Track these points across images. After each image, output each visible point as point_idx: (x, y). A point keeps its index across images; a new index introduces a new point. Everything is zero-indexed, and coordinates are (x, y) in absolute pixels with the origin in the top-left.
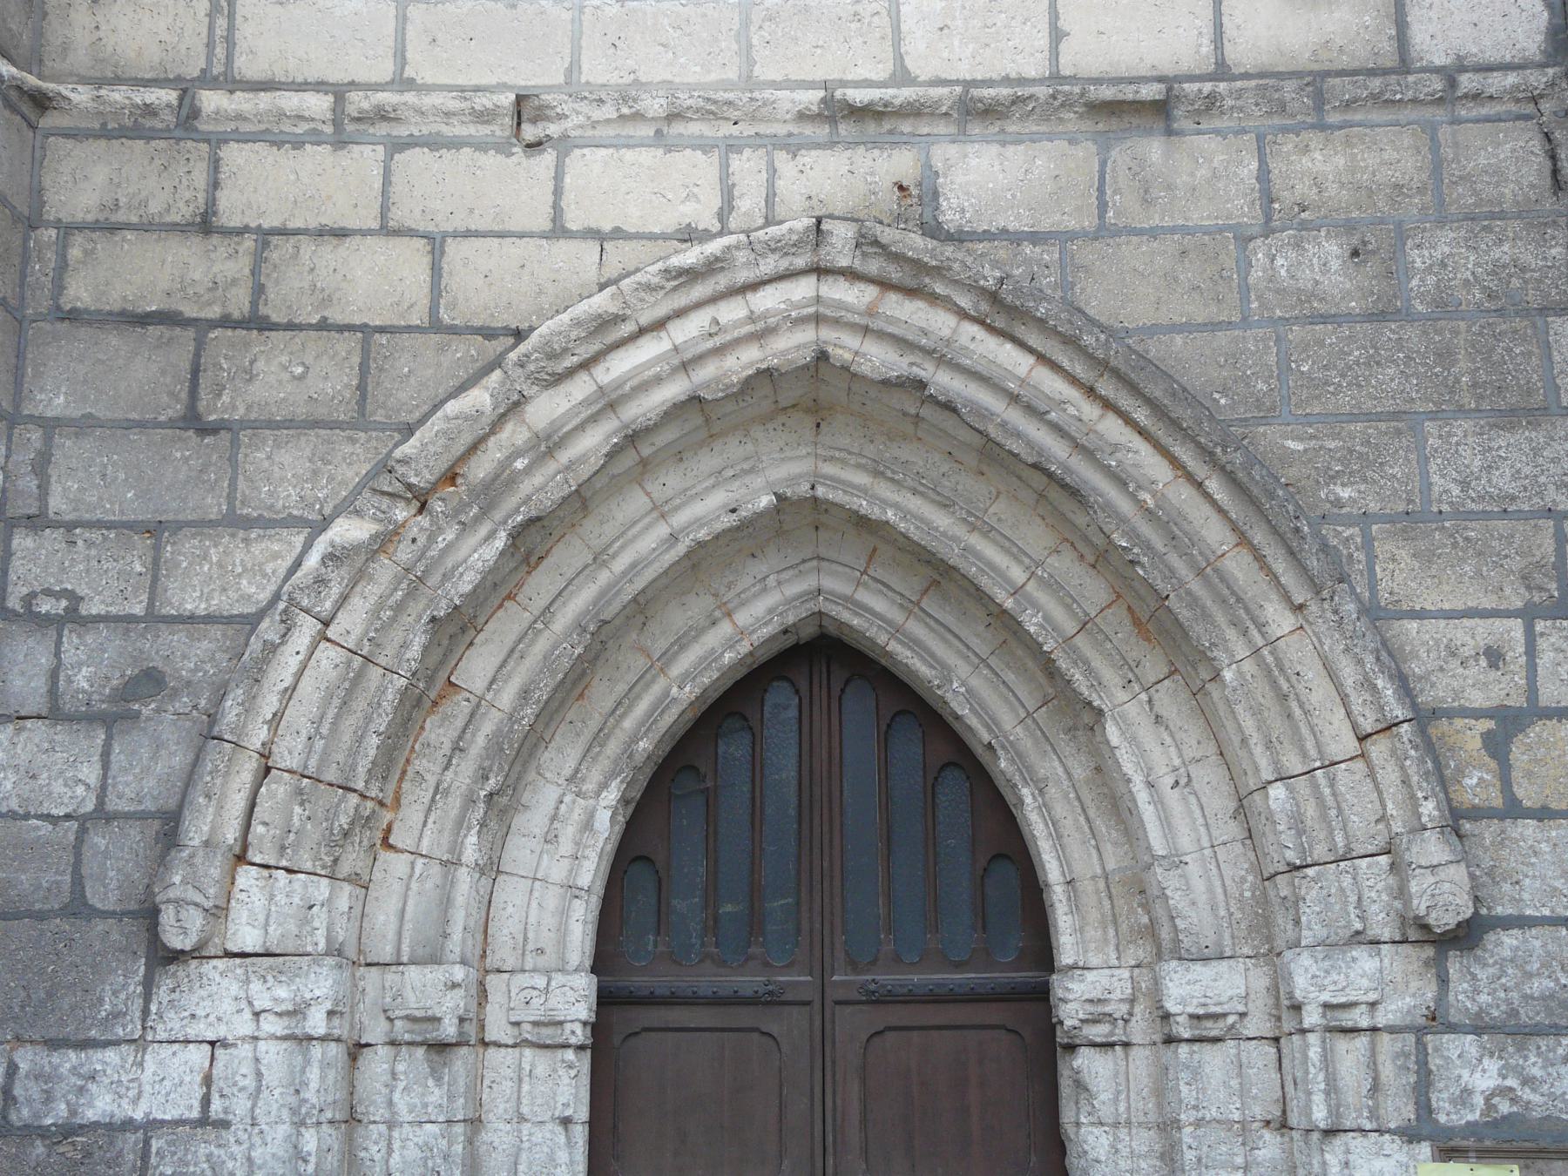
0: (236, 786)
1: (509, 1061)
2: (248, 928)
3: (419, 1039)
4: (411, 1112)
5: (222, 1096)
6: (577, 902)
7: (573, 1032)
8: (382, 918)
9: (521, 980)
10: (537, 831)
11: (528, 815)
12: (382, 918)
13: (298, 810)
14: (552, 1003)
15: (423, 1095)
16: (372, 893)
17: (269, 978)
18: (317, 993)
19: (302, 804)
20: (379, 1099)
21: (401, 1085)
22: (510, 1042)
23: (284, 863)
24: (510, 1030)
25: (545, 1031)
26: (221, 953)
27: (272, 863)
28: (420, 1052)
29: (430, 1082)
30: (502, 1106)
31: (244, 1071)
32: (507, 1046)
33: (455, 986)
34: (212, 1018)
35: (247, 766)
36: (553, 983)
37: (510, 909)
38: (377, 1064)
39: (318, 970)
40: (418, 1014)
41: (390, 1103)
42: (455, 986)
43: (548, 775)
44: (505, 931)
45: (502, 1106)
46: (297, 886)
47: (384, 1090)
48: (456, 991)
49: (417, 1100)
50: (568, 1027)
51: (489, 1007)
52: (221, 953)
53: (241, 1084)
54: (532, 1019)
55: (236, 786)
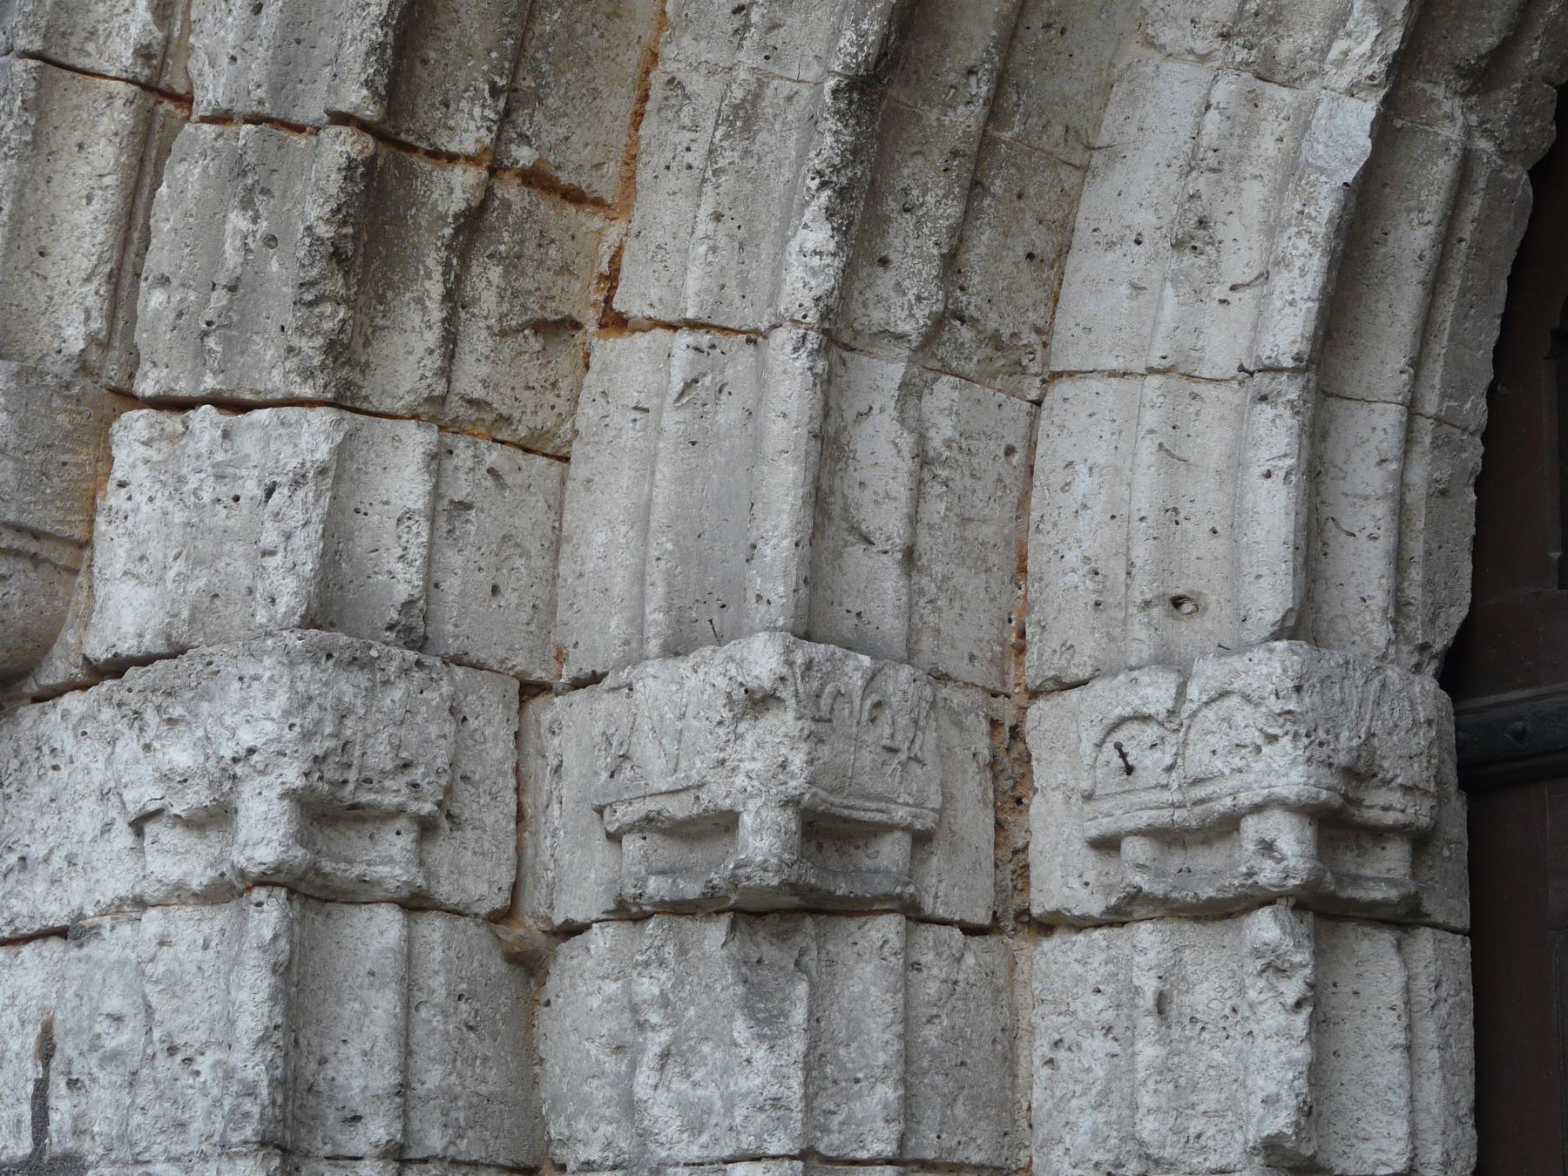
0: (77, 187)
1: (1097, 970)
2: (127, 587)
3: (692, 889)
4: (695, 1128)
5: (72, 1084)
6: (1266, 411)
7: (1267, 847)
8: (600, 538)
9: (1110, 698)
10: (1144, 220)
11: (1118, 178)
12: (600, 538)
13: (237, 221)
14: (1198, 759)
15: (726, 1071)
16: (578, 471)
17: (150, 716)
18: (247, 738)
19: (246, 204)
20: (599, 1092)
21: (656, 1042)
22: (1095, 906)
23: (210, 383)
24: (1091, 863)
25: (1206, 860)
26: (79, 675)
27: (183, 388)
28: (714, 934)
29: (741, 1029)
30: (1085, 1122)
31: (113, 1003)
32: (1081, 924)
33: (758, 702)
34: (58, 861)
35: (106, 124)
36: (1193, 691)
37: (1083, 484)
38: (592, 987)
39: (250, 669)
40: (679, 808)
41: (631, 1108)
42: (758, 702)
43: (1166, 36)
44: (1073, 557)
45: (1085, 1122)
46: (248, 444)
47: (611, 1064)
48: (770, 720)
49: (711, 1092)
50: (1252, 827)
51: (1036, 805)
52: (79, 675)
53: (110, 1044)
54: (1144, 819)
55: (77, 187)
